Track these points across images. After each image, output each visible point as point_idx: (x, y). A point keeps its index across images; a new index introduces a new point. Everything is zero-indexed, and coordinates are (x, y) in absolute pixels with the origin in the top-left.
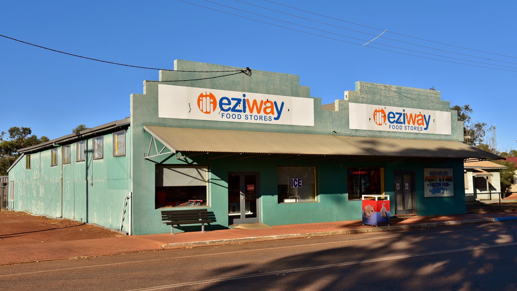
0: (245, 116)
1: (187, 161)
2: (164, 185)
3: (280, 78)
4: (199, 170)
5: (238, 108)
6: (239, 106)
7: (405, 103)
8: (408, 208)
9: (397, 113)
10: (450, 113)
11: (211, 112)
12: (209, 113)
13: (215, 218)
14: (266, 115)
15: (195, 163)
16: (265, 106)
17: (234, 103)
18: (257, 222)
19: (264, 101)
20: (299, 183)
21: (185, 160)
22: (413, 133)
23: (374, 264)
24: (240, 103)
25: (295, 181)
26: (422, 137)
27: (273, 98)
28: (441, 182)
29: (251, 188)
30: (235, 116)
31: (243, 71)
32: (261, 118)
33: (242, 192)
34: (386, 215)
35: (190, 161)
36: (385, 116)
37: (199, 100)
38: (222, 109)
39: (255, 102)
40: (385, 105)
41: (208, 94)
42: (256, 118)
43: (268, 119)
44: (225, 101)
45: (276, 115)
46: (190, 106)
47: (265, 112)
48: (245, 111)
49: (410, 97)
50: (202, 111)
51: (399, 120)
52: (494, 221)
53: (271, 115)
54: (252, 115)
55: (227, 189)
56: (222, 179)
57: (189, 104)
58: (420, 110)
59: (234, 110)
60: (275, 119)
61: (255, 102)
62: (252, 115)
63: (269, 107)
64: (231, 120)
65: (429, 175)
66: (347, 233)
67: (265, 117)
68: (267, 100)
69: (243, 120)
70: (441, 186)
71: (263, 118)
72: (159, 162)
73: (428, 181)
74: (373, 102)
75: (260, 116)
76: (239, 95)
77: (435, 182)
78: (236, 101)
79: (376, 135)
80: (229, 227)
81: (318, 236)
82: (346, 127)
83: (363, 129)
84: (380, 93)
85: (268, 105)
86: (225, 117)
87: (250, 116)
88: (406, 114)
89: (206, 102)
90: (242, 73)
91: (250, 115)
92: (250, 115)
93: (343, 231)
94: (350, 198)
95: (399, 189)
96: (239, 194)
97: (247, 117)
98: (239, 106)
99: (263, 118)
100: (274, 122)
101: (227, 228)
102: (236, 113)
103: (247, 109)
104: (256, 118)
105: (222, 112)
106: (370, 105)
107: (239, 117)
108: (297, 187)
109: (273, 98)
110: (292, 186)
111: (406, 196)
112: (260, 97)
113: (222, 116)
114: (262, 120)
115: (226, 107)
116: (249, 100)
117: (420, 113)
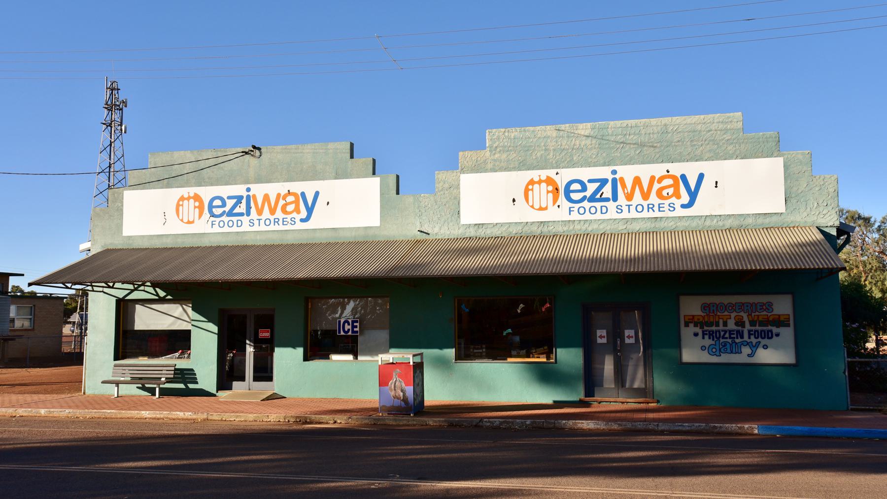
0: (250, 221)
1: (157, 295)
2: (135, 329)
3: (314, 153)
4: (184, 306)
5: (237, 210)
6: (240, 206)
7: (619, 155)
8: (636, 385)
10: (780, 160)
11: (195, 222)
12: (193, 222)
13: (196, 379)
14: (285, 216)
15: (169, 297)
16: (284, 202)
17: (230, 203)
18: (76, 384)
19: (282, 195)
20: (354, 327)
21: (155, 294)
22: (277, 231)
23: (417, 486)
24: (241, 203)
25: (346, 324)
26: (674, 226)
27: (677, 169)
29: (265, 334)
30: (224, 223)
31: (246, 153)
32: (277, 222)
33: (250, 341)
34: (404, 395)
35: (162, 294)
36: (557, 189)
37: (178, 205)
38: (213, 215)
39: (266, 197)
40: (557, 167)
41: (192, 195)
42: (268, 222)
43: (290, 221)
44: (217, 202)
45: (304, 214)
46: (165, 216)
47: (284, 210)
48: (248, 214)
49: (634, 142)
50: (182, 220)
51: (600, 194)
52: (756, 432)
53: (294, 215)
54: (261, 219)
55: (216, 336)
56: (210, 320)
57: (164, 213)
58: (668, 166)
59: (231, 214)
60: (302, 220)
61: (266, 197)
62: (261, 219)
63: (291, 203)
64: (226, 229)
66: (287, 420)
67: (285, 220)
68: (289, 191)
69: (246, 228)
71: (281, 222)
72: (121, 297)
74: (523, 166)
75: (648, 205)
76: (239, 190)
78: (235, 201)
79: (529, 231)
80: (217, 394)
81: (224, 419)
82: (451, 221)
83: (495, 222)
84: (544, 146)
85: (290, 199)
86: (216, 227)
87: (258, 221)
88: (254, 196)
89: (189, 207)
90: (247, 156)
91: (257, 219)
92: (257, 219)
93: (277, 416)
94: (459, 357)
95: (606, 342)
96: (246, 344)
97: (619, 209)
98: (240, 206)
99: (281, 222)
100: (680, 212)
101: (214, 395)
102: (235, 219)
103: (253, 210)
104: (268, 222)
105: (212, 219)
106: (514, 173)
107: (239, 224)
108: (350, 333)
109: (297, 187)
110: (340, 332)
111: (632, 359)
112: (274, 189)
113: (212, 224)
114: (279, 225)
115: (575, 196)
116: (625, 179)
117: (668, 172)
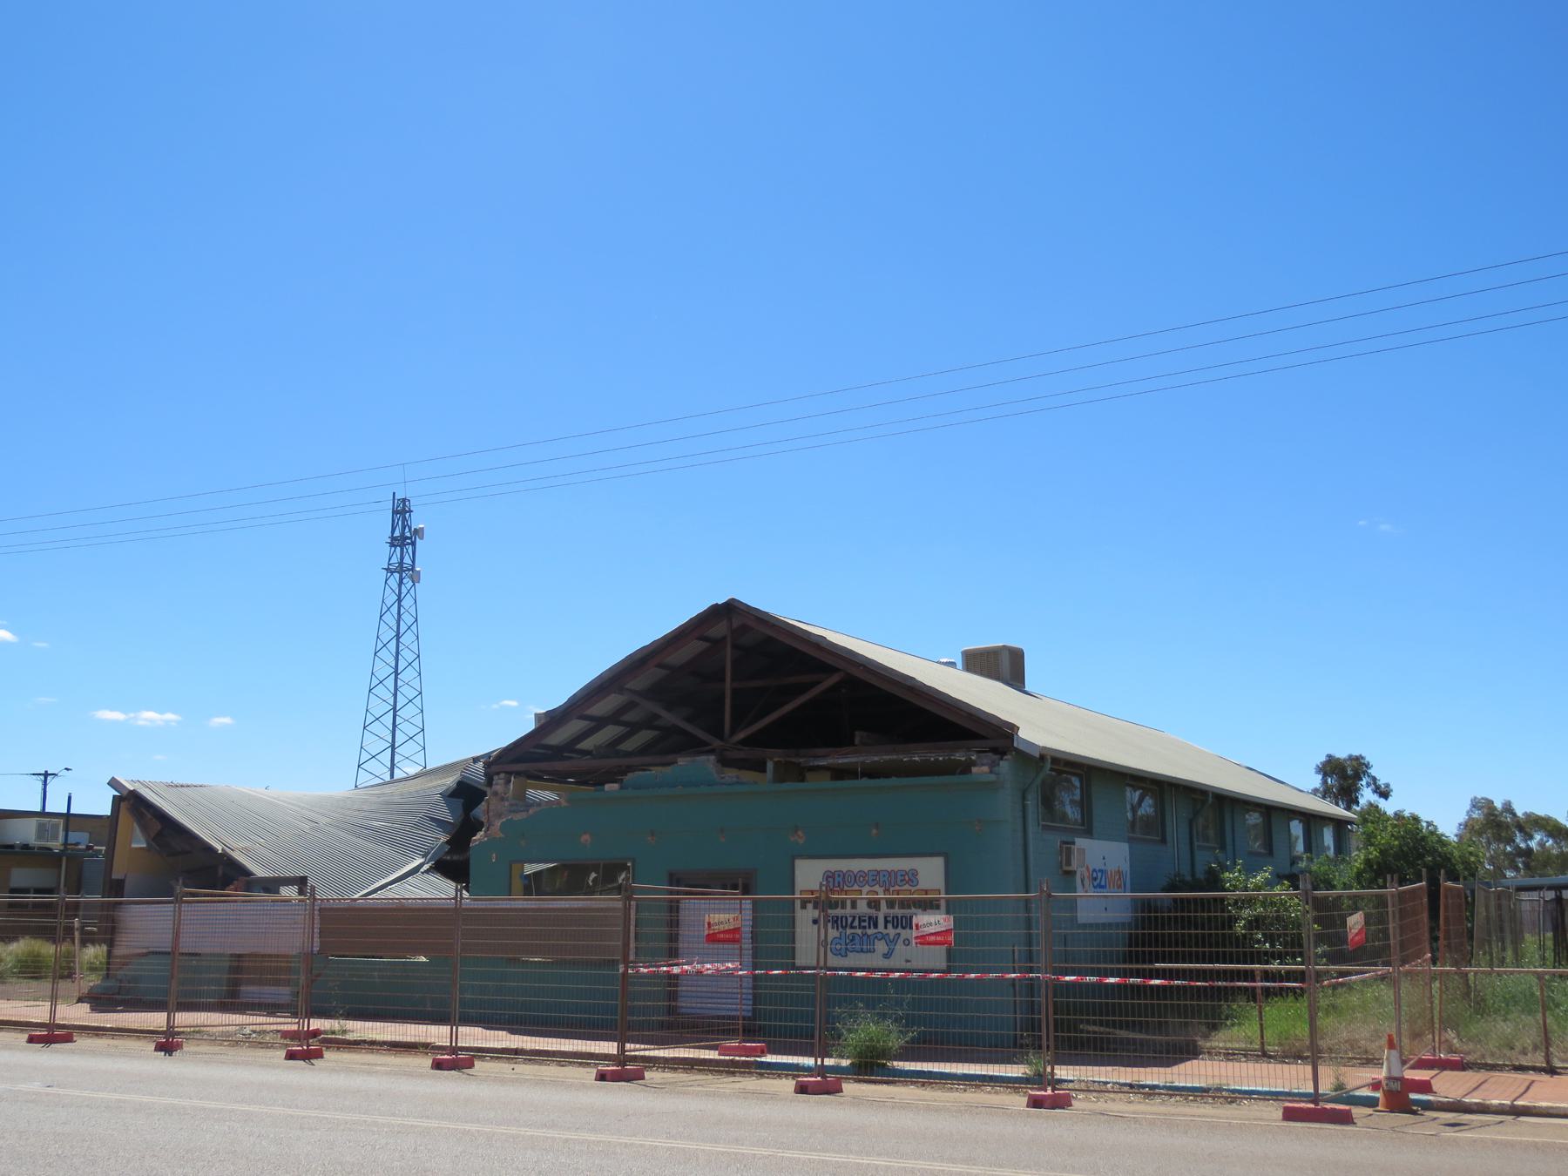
70: (876, 926)
77: (848, 911)
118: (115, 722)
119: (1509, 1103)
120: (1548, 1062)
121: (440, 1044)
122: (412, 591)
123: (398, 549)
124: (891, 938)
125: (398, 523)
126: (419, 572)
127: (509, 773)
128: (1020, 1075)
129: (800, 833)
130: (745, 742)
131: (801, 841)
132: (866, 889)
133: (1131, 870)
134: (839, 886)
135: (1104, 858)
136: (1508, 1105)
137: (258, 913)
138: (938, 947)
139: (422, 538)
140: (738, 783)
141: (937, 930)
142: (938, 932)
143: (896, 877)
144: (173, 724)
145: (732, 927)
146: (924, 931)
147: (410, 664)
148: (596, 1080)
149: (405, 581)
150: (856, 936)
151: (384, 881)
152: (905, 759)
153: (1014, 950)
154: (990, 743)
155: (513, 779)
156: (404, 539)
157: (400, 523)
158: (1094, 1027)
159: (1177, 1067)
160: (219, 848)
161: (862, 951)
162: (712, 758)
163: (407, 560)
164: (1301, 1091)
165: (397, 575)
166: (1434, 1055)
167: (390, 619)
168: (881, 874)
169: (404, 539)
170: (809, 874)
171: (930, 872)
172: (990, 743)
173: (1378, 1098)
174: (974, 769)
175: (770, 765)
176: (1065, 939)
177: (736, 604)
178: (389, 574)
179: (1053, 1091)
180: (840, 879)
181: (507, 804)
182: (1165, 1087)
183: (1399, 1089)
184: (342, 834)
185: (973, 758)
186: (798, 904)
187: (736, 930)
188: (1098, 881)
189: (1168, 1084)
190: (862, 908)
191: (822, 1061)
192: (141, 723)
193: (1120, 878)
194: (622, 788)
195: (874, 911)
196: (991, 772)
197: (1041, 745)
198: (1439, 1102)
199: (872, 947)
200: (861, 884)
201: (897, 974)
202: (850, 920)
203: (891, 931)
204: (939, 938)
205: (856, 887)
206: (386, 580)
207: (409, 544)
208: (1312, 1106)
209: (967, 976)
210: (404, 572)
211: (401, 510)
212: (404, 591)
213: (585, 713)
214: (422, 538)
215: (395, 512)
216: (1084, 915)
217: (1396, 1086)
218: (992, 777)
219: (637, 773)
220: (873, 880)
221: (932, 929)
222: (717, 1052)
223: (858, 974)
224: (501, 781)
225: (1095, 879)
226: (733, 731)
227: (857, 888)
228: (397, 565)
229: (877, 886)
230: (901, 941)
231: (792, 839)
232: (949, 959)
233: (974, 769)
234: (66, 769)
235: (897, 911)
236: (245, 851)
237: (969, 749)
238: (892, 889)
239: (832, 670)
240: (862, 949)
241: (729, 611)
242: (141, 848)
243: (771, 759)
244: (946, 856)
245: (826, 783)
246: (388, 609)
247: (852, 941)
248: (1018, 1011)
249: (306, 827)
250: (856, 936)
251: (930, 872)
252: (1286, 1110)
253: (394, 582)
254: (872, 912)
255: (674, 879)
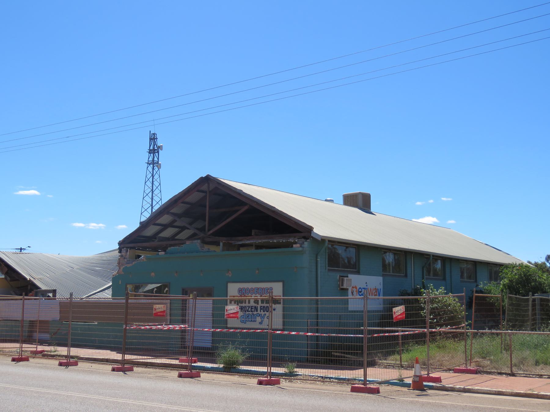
9: (363, 288)
28: (258, 304)
65: (236, 293)
70: (257, 311)
73: (235, 303)
77: (247, 304)
118: (80, 228)
119: (462, 387)
120: (511, 371)
121: (82, 357)
122: (158, 172)
123: (152, 154)
124: (263, 316)
125: (152, 143)
126: (160, 164)
127: (127, 248)
128: (283, 372)
129: (230, 272)
130: (214, 234)
131: (230, 276)
132: (254, 295)
133: (383, 288)
134: (244, 294)
135: (366, 283)
136: (462, 388)
137: (33, 304)
138: (233, 319)
139: (162, 150)
140: (208, 251)
141: (233, 312)
142: (233, 313)
143: (265, 290)
144: (103, 228)
145: (162, 310)
146: (229, 312)
147: (158, 203)
148: (111, 371)
149: (155, 168)
150: (250, 315)
151: (95, 292)
152: (271, 241)
153: (308, 321)
154: (303, 235)
155: (129, 250)
156: (154, 150)
157: (153, 143)
158: (349, 355)
159: (358, 370)
160: (28, 278)
161: (251, 321)
162: (199, 241)
163: (156, 159)
164: (329, 376)
165: (152, 165)
166: (466, 368)
167: (149, 184)
168: (259, 289)
169: (154, 150)
170: (233, 289)
171: (277, 289)
172: (303, 235)
173: (411, 383)
174: (294, 246)
175: (221, 244)
176: (340, 318)
177: (209, 177)
178: (148, 165)
179: (270, 378)
180: (244, 291)
181: (126, 260)
182: (336, 378)
183: (418, 380)
184: (83, 273)
185: (296, 241)
186: (229, 301)
187: (164, 312)
188: (362, 293)
189: (336, 377)
190: (252, 304)
191: (270, 369)
192: (90, 227)
193: (376, 292)
194: (166, 254)
195: (256, 304)
196: (301, 247)
197: (322, 235)
198: (436, 386)
199: (255, 319)
200: (248, 294)
201: (259, 331)
202: (247, 308)
203: (262, 313)
204: (234, 315)
205: (250, 295)
206: (147, 168)
207: (156, 152)
208: (363, 386)
209: (243, 331)
210: (154, 164)
211: (153, 138)
212: (155, 172)
213: (156, 222)
214: (162, 150)
215: (151, 139)
216: (352, 306)
217: (417, 379)
218: (301, 249)
219: (171, 247)
220: (256, 292)
221: (232, 312)
222: (178, 361)
223: (278, 332)
224: (125, 251)
225: (361, 292)
226: (209, 230)
227: (251, 295)
228: (151, 161)
229: (258, 294)
230: (266, 317)
231: (227, 275)
232: (284, 325)
233: (294, 246)
234: (28, 247)
235: (265, 305)
236: (40, 280)
237: (295, 237)
238: (263, 295)
239: (243, 204)
240: (252, 320)
241: (207, 180)
242: (2, 278)
243: (222, 242)
244: (283, 282)
245: (253, 251)
246: (148, 179)
247: (248, 317)
248: (309, 347)
249: (68, 270)
250: (250, 315)
251: (277, 289)
252: (352, 387)
253: (150, 168)
254: (256, 305)
255: (185, 292)
